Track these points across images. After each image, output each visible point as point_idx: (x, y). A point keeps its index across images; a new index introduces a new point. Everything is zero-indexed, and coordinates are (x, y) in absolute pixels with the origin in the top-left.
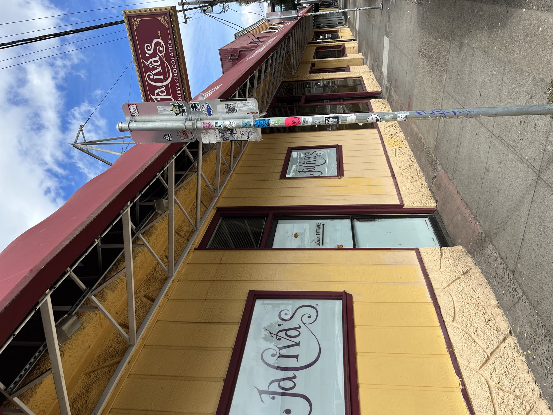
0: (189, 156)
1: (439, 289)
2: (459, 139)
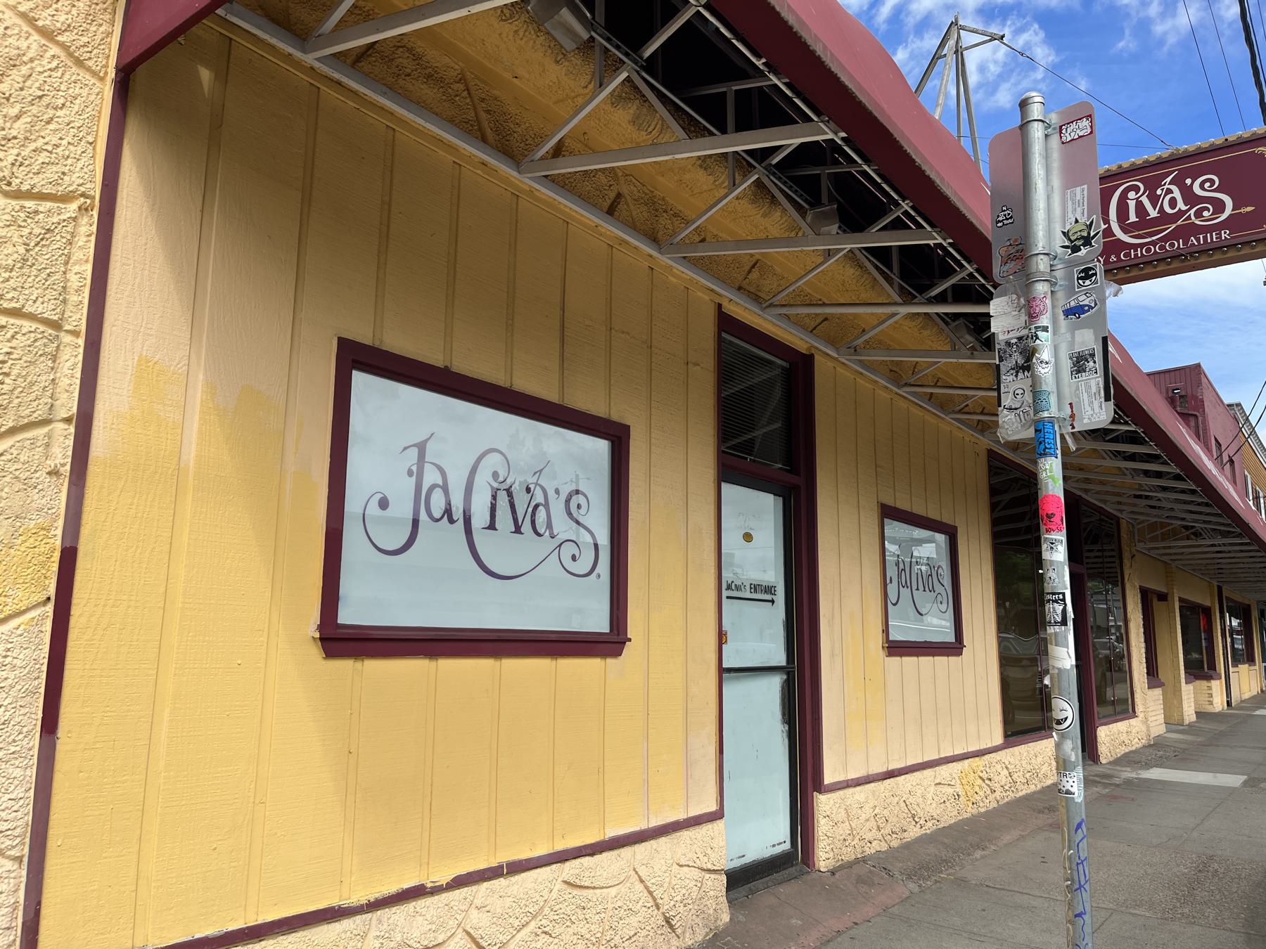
0: (938, 288)
1: (634, 858)
2: (991, 937)
